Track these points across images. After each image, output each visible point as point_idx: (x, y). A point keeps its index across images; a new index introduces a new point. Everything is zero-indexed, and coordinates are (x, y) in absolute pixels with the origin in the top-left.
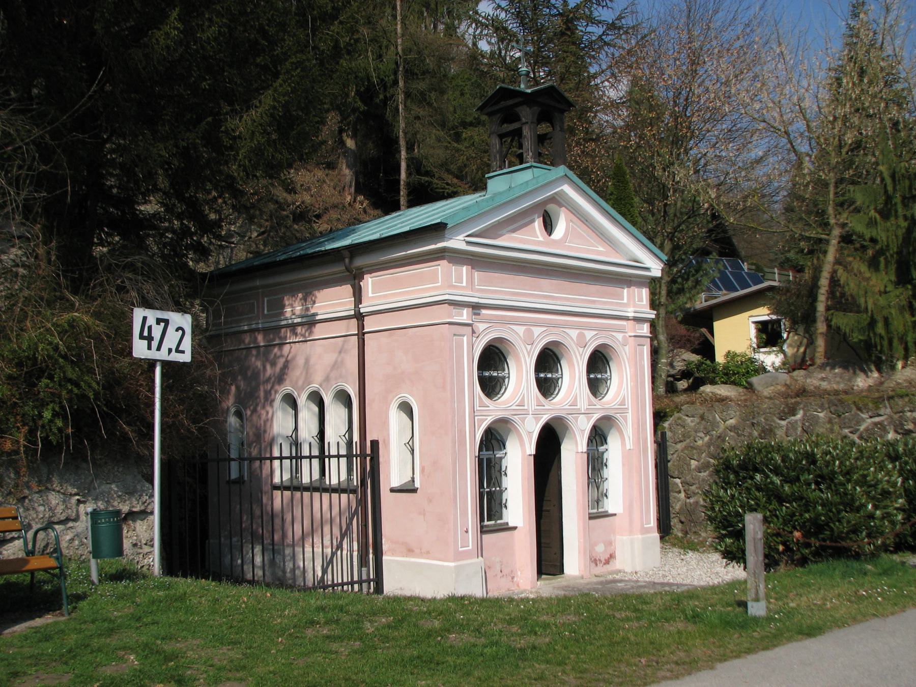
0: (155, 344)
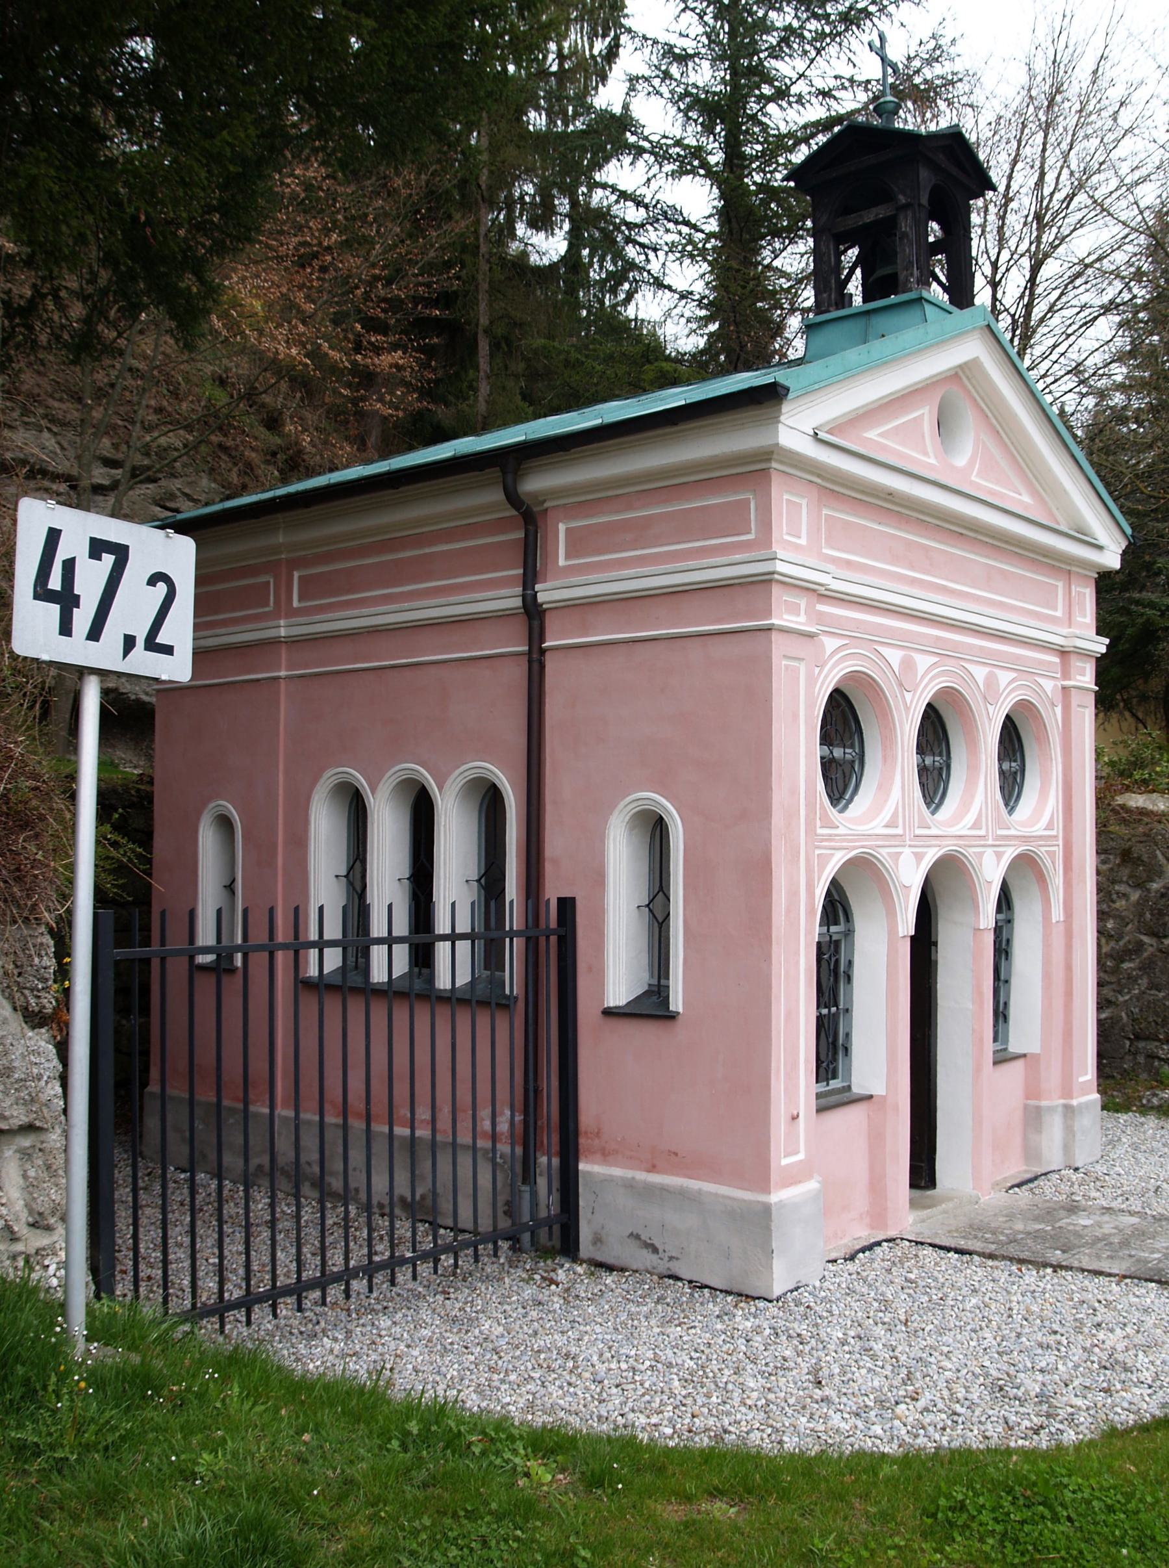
0: (83, 618)
